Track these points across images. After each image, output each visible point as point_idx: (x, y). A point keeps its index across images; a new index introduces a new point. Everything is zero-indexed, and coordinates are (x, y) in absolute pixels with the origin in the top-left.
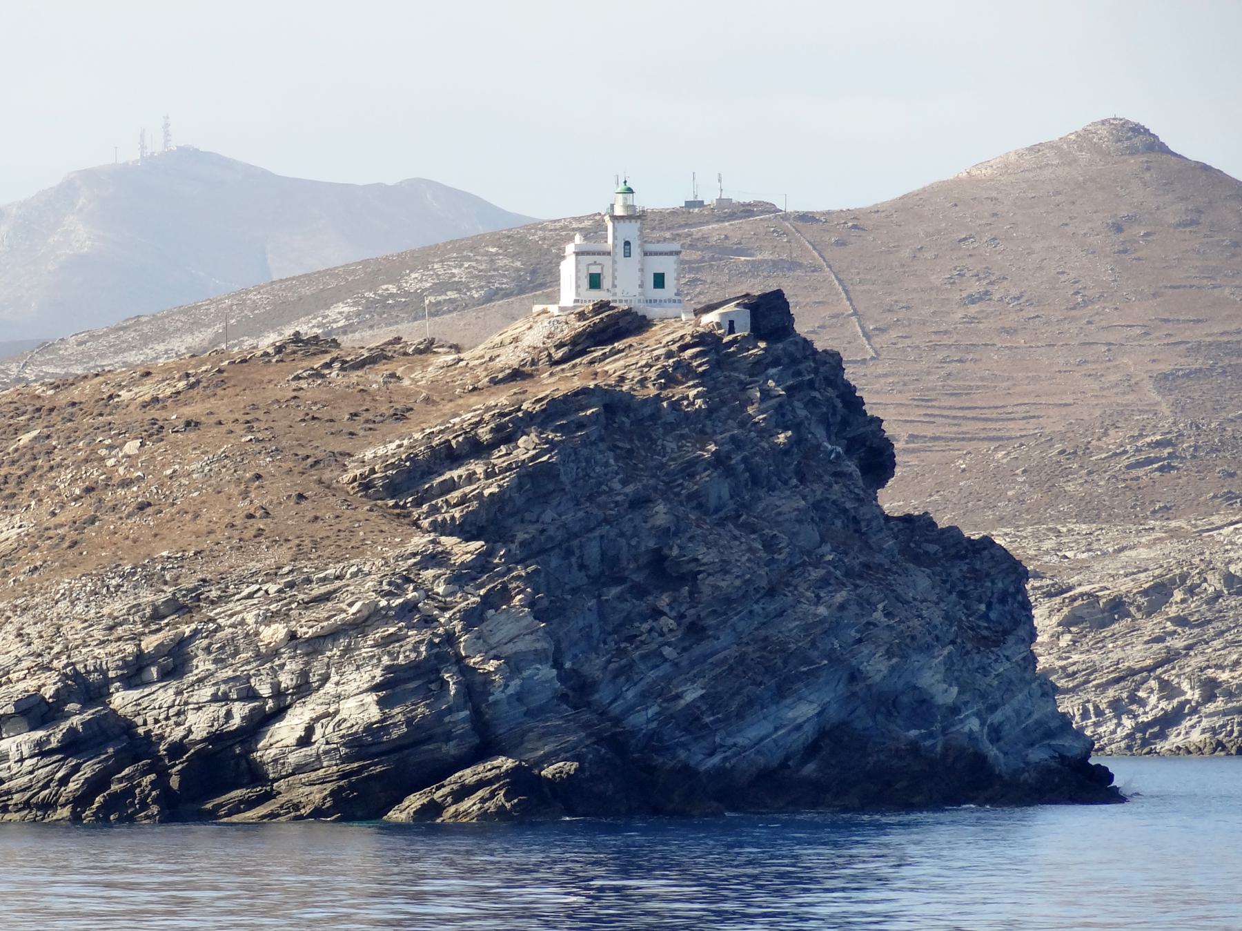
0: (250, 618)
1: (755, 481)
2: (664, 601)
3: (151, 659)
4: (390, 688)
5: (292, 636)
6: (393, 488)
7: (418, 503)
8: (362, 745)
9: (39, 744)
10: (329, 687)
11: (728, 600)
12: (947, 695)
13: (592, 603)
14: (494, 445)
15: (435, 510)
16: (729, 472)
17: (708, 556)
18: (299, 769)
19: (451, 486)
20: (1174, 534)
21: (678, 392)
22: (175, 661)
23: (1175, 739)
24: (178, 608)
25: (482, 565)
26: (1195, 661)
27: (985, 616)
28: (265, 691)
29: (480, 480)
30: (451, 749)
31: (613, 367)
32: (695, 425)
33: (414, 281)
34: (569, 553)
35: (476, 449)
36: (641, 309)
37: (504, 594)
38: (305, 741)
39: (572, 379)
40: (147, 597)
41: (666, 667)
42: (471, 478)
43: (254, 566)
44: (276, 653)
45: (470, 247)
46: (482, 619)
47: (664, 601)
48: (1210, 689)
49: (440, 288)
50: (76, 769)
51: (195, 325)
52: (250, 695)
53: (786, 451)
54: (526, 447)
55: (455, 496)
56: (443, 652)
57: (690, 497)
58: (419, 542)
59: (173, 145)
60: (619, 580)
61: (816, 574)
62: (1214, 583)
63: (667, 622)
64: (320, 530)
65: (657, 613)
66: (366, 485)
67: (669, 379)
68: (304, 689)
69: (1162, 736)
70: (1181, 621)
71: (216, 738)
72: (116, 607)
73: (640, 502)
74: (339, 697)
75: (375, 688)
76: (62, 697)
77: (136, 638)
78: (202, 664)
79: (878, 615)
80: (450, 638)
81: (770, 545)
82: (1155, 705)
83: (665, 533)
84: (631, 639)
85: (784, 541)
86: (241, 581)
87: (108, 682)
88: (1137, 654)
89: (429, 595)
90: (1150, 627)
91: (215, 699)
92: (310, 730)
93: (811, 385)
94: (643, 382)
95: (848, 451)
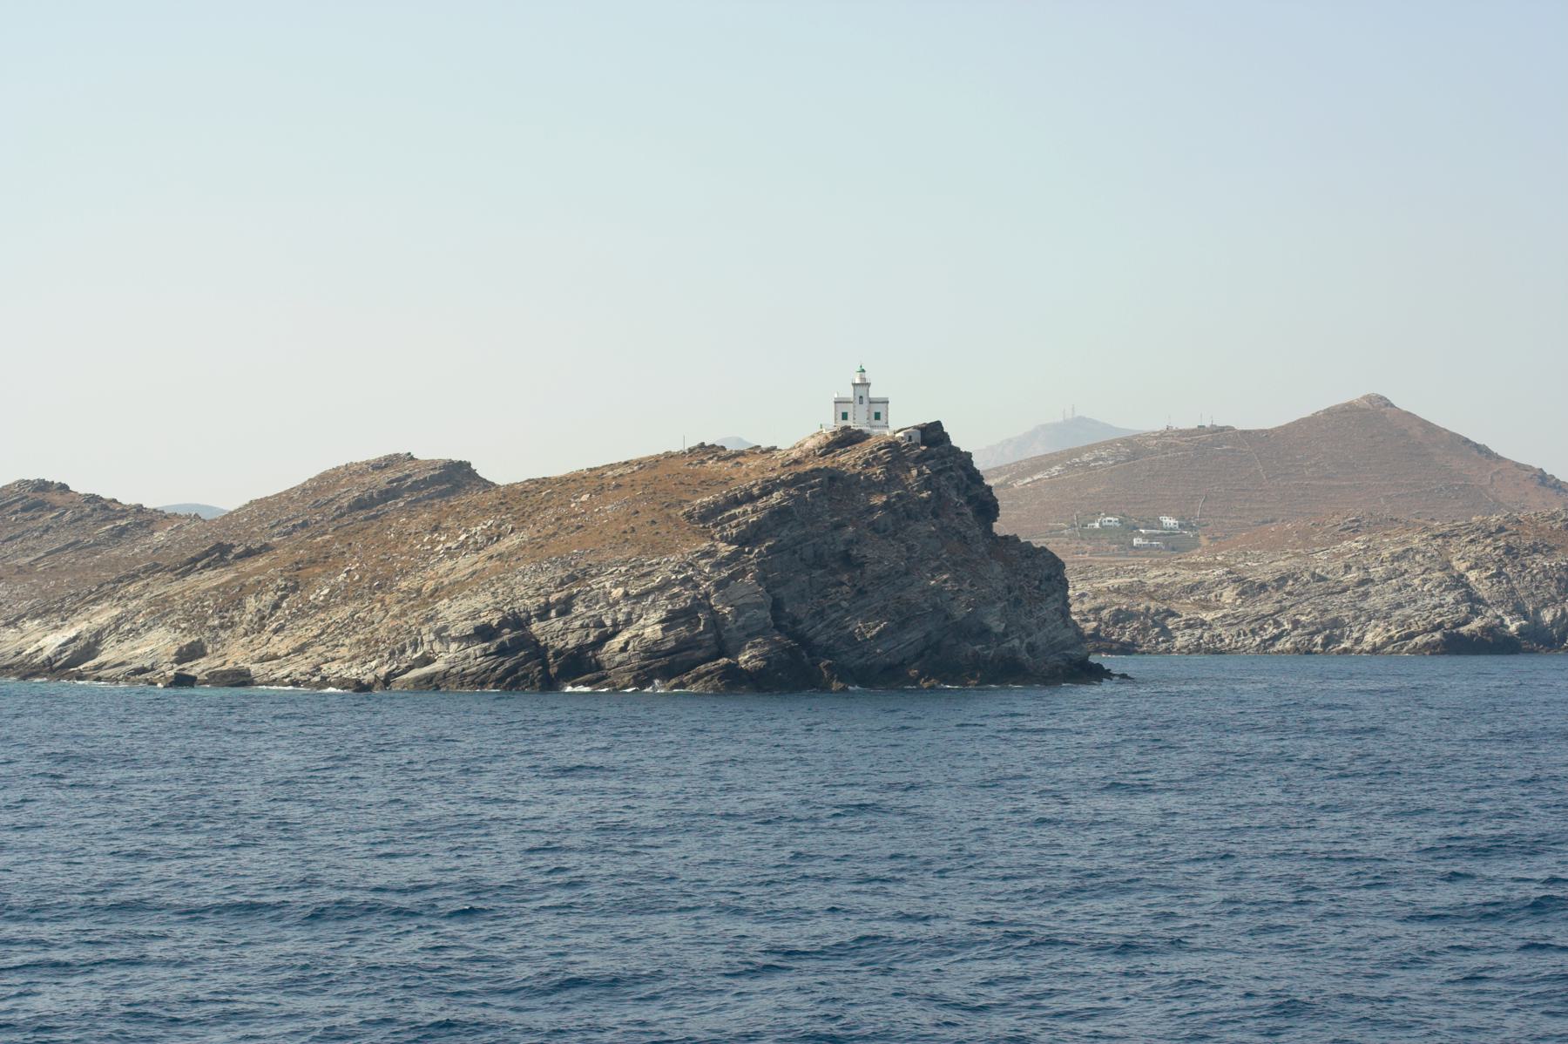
0: (608, 584)
1: (909, 517)
2: (845, 578)
3: (553, 606)
4: (669, 621)
5: (626, 594)
6: (704, 518)
7: (715, 526)
8: (651, 651)
9: (485, 649)
10: (642, 622)
11: (879, 578)
12: (998, 626)
13: (805, 578)
14: (760, 497)
15: (724, 529)
16: (894, 512)
17: (870, 553)
18: (620, 664)
19: (734, 517)
20: (1296, 555)
21: (870, 471)
22: (565, 608)
23: (1279, 646)
24: (572, 578)
25: (733, 557)
26: (1293, 611)
27: (1038, 588)
28: (608, 622)
29: (748, 514)
30: (699, 654)
31: (842, 459)
32: (872, 486)
33: (1086, 457)
34: (795, 552)
35: (751, 498)
36: (866, 429)
37: (744, 573)
38: (623, 650)
39: (824, 463)
40: (560, 573)
41: (842, 612)
42: (745, 513)
43: (618, 557)
44: (617, 603)
45: (1111, 443)
46: (727, 585)
47: (845, 578)
48: (1296, 624)
49: (1096, 460)
50: (502, 663)
51: (1000, 474)
52: (601, 624)
53: (927, 501)
54: (776, 497)
55: (734, 523)
56: (701, 603)
57: (869, 524)
58: (705, 545)
59: (1077, 414)
60: (824, 567)
61: (934, 564)
62: (1307, 576)
63: (845, 588)
64: (658, 538)
65: (842, 584)
66: (689, 516)
67: (867, 464)
68: (628, 622)
69: (1273, 645)
70: (1290, 593)
71: (581, 648)
72: (543, 579)
73: (838, 527)
74: (644, 627)
75: (661, 622)
76: (504, 623)
77: (548, 594)
78: (579, 608)
79: (966, 586)
80: (707, 596)
81: (910, 549)
82: (1272, 630)
83: (849, 542)
84: (825, 597)
85: (919, 547)
86: (609, 565)
87: (530, 617)
88: (1267, 608)
89: (700, 572)
90: (1277, 596)
91: (582, 626)
92: (627, 643)
93: (951, 469)
94: (854, 466)
95: (968, 503)
